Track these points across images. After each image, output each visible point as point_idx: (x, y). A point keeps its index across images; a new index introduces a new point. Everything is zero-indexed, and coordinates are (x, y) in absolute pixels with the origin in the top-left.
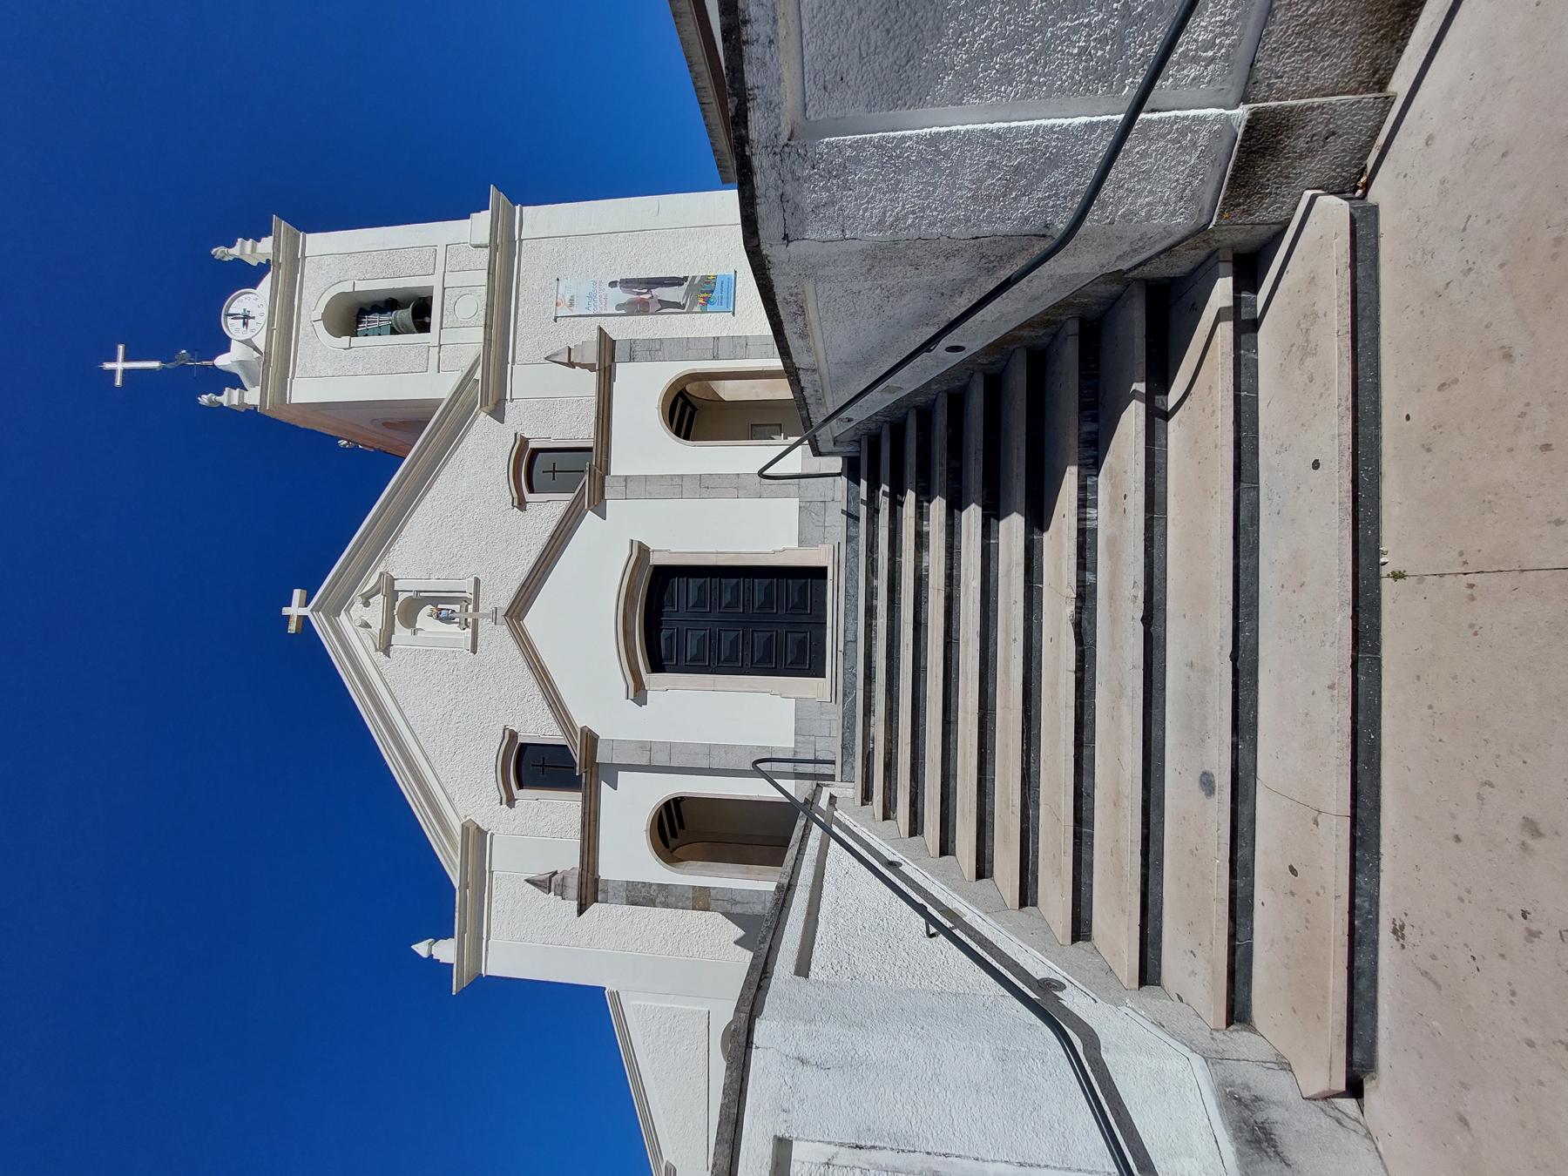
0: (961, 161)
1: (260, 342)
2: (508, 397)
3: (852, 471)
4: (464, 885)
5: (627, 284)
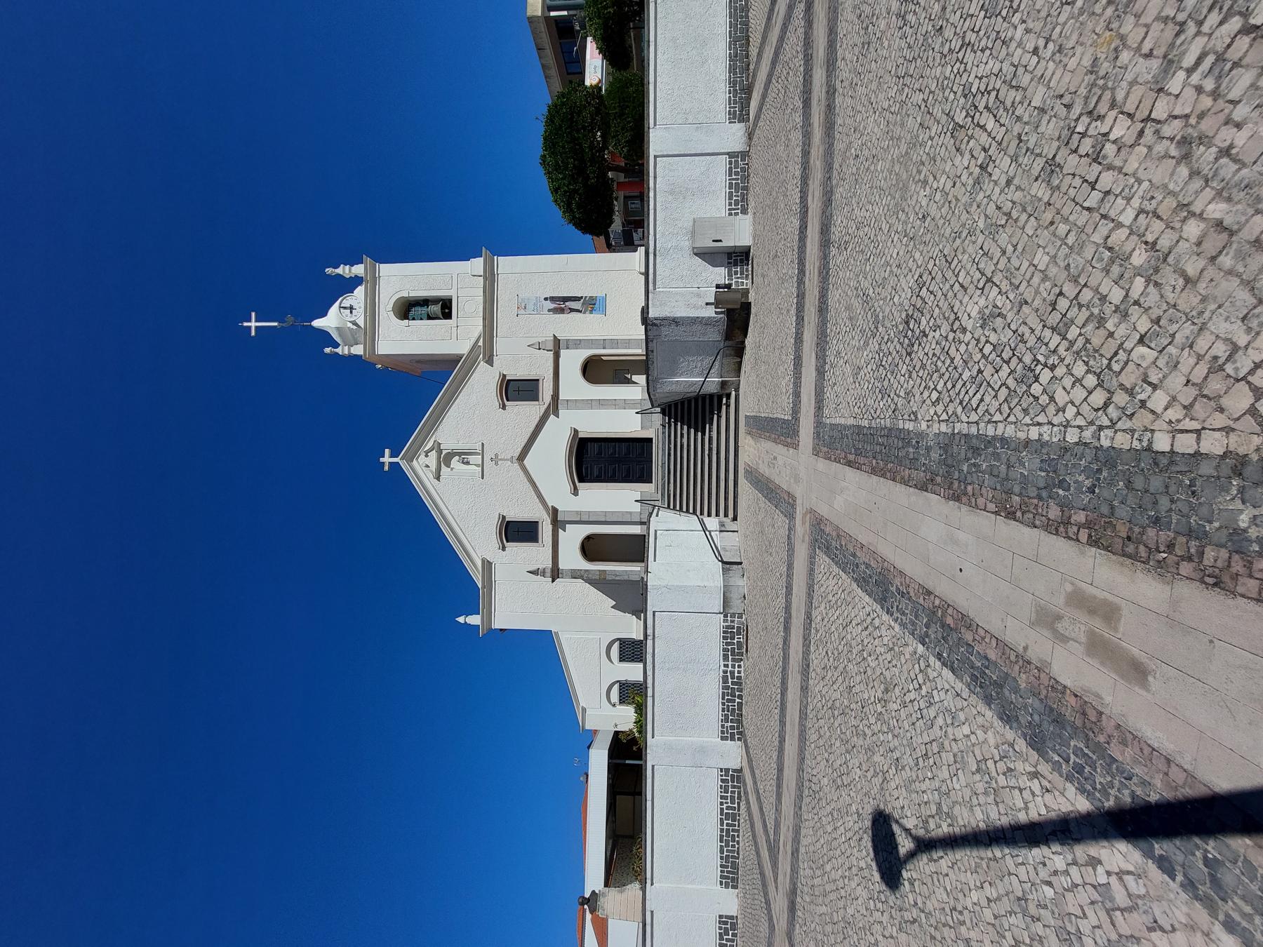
1: (361, 322)
3: (663, 412)
4: (484, 587)
5: (553, 299)
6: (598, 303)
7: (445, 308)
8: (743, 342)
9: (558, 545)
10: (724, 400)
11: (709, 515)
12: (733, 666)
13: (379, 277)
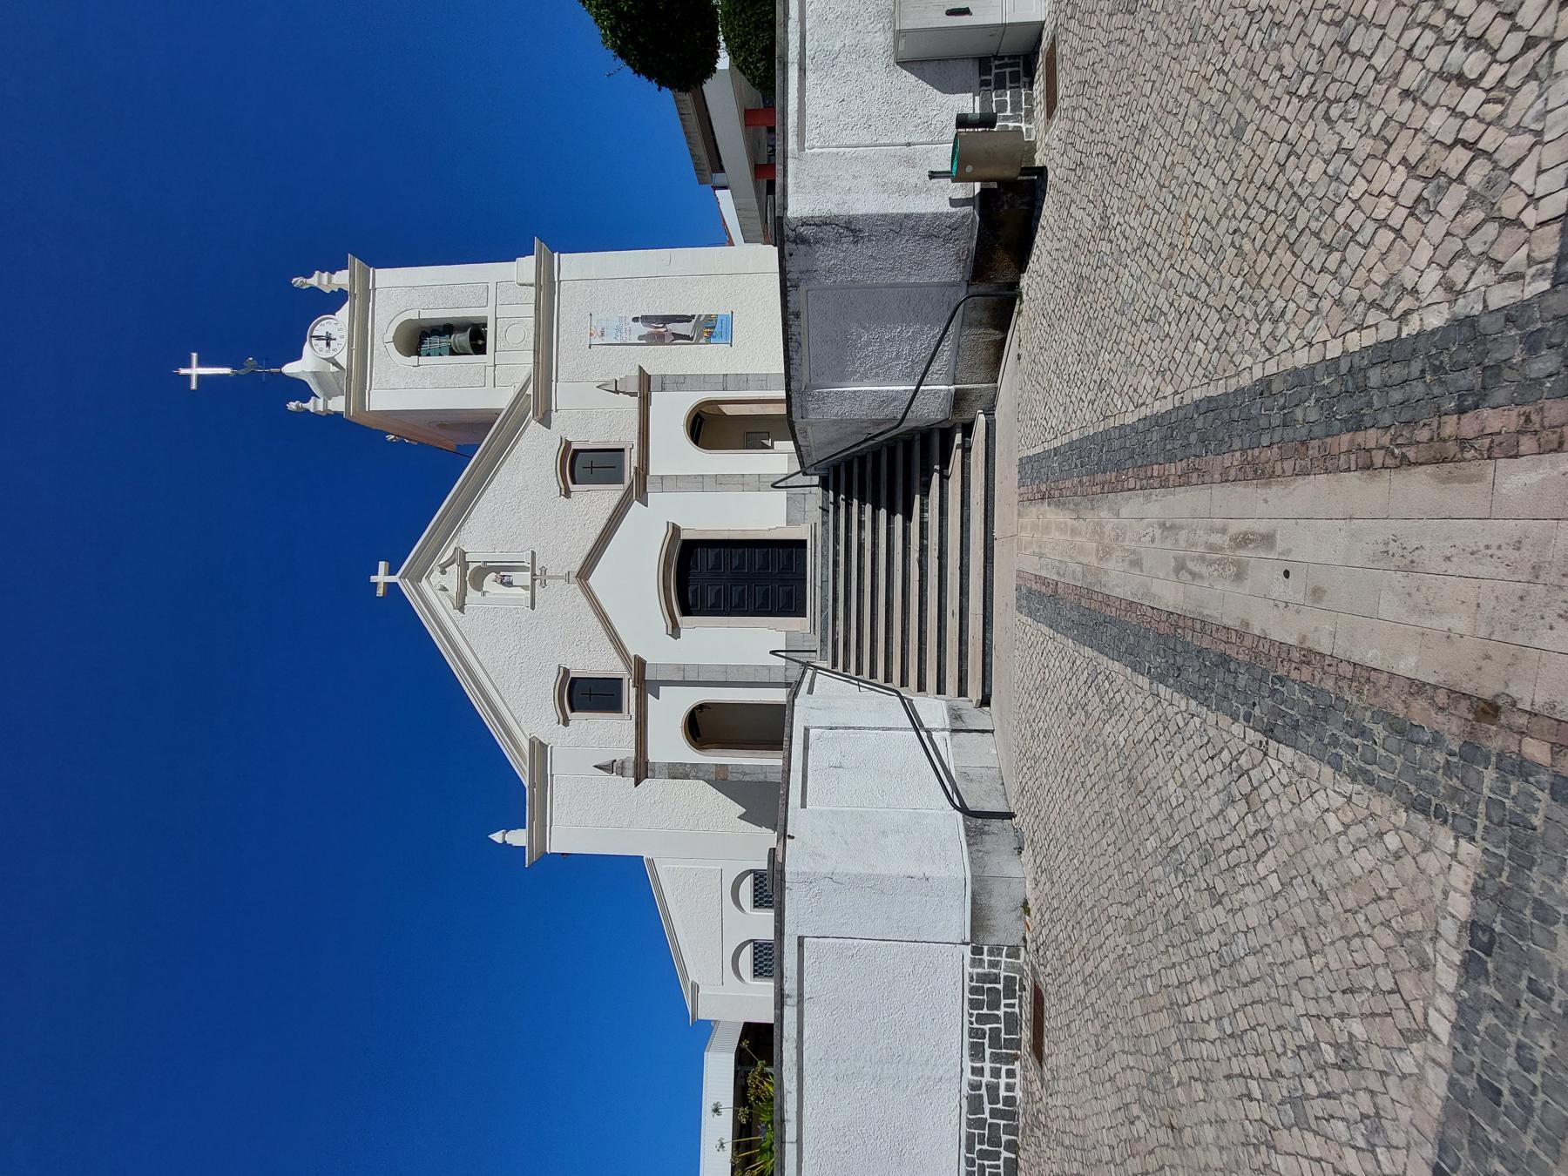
0: (864, 398)
1: (342, 359)
2: (553, 408)
3: (824, 484)
4: (532, 785)
5: (646, 319)
6: (719, 325)
7: (476, 338)
8: (1014, 285)
9: (646, 725)
10: (958, 438)
11: (921, 687)
12: (996, 1073)
13: (375, 289)
